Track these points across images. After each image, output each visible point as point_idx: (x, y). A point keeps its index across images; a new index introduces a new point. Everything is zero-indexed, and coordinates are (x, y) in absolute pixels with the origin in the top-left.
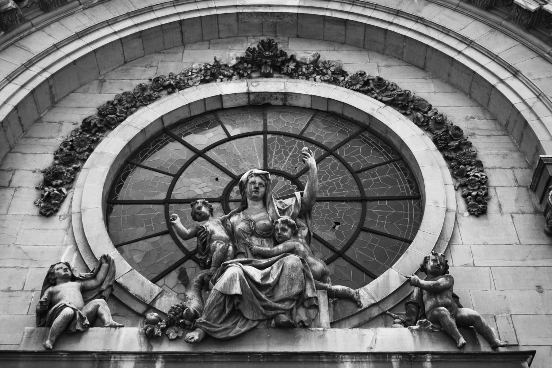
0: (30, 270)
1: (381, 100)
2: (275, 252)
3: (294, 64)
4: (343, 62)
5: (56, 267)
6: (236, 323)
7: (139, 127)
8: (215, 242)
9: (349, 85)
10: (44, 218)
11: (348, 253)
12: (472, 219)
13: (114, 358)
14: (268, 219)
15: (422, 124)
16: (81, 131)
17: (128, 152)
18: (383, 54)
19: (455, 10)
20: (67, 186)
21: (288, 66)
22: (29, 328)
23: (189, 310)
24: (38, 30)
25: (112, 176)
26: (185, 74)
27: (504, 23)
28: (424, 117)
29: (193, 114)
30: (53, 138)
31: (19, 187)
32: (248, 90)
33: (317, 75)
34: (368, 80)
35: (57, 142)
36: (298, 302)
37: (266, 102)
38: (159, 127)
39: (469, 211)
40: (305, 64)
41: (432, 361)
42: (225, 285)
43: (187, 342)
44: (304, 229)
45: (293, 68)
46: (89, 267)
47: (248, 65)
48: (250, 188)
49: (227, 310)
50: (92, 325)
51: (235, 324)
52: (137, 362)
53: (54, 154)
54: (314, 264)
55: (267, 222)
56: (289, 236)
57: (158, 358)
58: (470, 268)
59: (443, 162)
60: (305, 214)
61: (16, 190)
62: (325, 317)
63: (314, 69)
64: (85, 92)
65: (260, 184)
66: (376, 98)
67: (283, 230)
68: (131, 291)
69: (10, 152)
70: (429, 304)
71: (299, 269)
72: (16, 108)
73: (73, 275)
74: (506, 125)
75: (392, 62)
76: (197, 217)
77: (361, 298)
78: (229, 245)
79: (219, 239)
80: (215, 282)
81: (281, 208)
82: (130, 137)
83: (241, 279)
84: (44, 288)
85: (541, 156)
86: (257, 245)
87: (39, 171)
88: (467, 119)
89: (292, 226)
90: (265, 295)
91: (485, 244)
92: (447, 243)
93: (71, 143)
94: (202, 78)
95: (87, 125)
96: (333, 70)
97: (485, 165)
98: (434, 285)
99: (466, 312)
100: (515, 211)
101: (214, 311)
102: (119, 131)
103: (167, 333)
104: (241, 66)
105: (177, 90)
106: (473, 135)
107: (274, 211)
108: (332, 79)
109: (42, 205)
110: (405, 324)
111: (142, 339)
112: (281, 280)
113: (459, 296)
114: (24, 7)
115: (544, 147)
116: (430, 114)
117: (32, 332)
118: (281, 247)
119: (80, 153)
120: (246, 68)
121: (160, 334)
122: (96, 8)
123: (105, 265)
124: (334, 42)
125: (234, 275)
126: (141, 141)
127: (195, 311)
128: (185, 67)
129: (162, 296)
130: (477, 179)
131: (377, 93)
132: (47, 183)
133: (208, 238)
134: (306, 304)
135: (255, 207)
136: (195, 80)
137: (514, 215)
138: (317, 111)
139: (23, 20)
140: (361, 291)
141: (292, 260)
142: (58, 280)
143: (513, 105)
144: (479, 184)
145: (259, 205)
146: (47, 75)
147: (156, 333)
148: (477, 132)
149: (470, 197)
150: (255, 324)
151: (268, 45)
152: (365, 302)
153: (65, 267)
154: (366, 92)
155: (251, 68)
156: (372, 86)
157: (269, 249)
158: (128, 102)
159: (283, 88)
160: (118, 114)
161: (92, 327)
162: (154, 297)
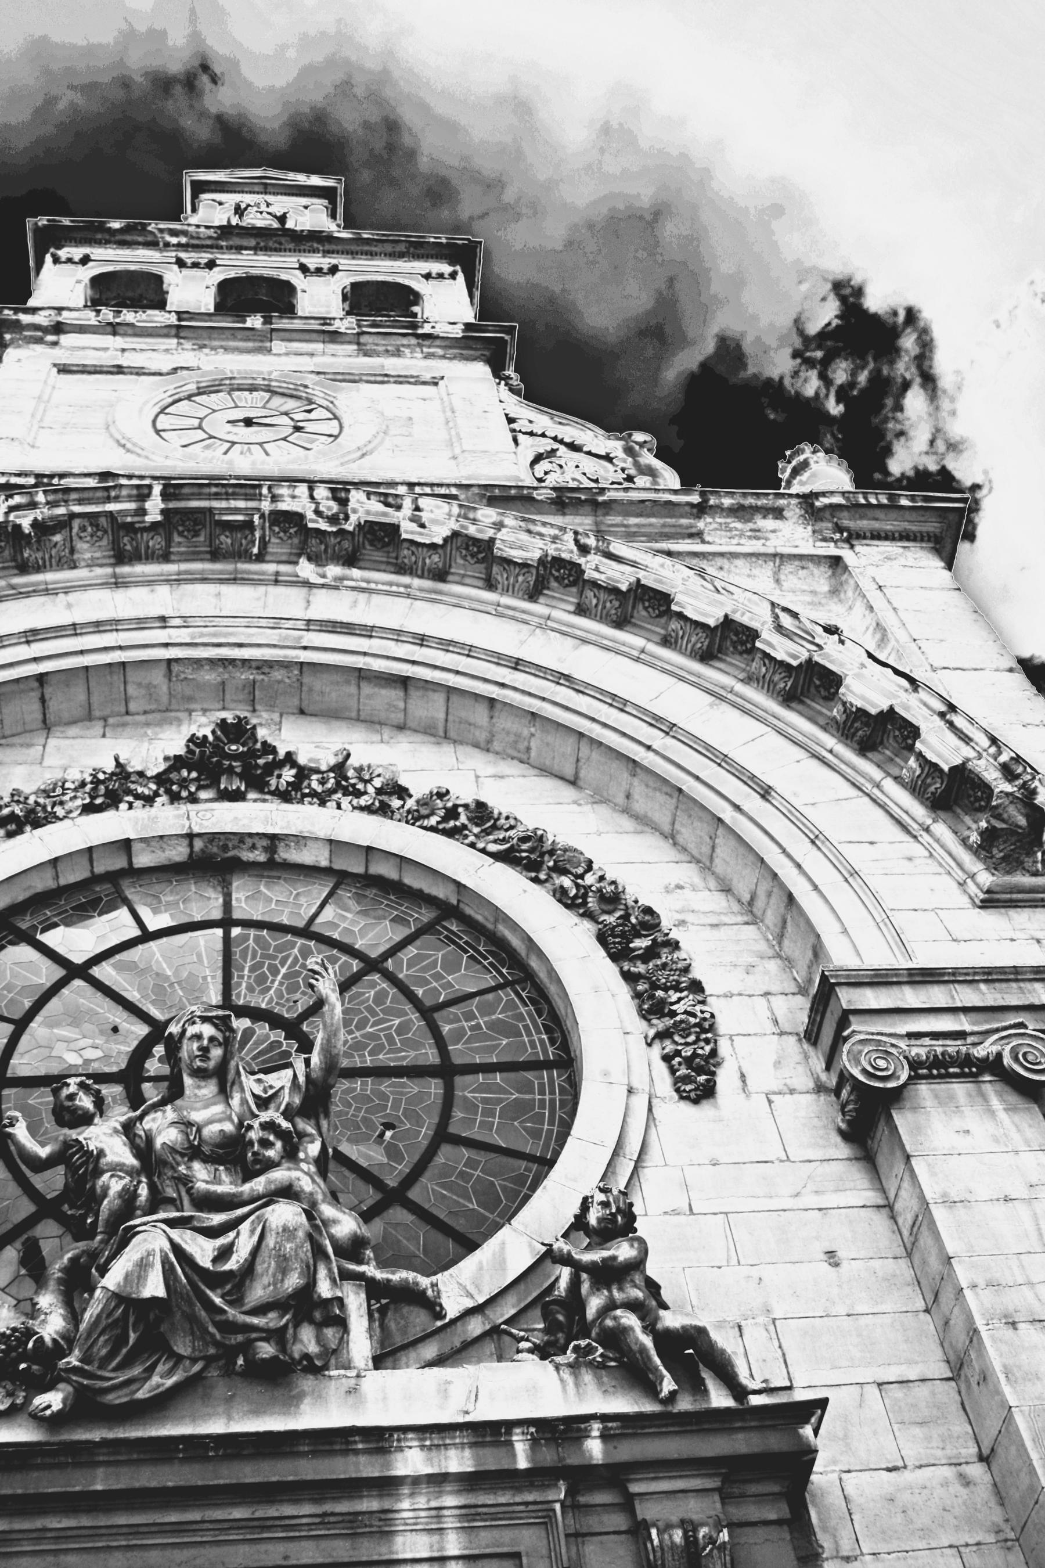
1: (483, 851)
2: (245, 1197)
3: (293, 772)
9: (414, 818)
18: (488, 750)
21: (279, 776)
28: (577, 886)
33: (344, 795)
40: (317, 771)
41: (604, 1437)
44: (312, 1142)
48: (188, 1049)
51: (150, 1371)
55: (229, 1127)
58: (682, 1219)
63: (338, 783)
65: (212, 1039)
66: (472, 845)
67: (265, 1144)
70: (594, 1304)
71: (301, 1234)
74: (751, 902)
76: (67, 1117)
78: (139, 1182)
79: (116, 1168)
80: (103, 1271)
83: (165, 1261)
90: (222, 1297)
92: (632, 1164)
94: (87, 801)
97: (708, 989)
101: (102, 1339)
104: (174, 776)
107: (244, 1102)
108: (377, 804)
110: (543, 1352)
112: (259, 1260)
116: (590, 879)
120: (185, 780)
127: (54, 1340)
131: (476, 835)
136: (70, 805)
145: (209, 1089)
148: (689, 918)
149: (678, 1059)
152: (453, 1307)
154: (450, 833)
155: (197, 779)
156: (463, 819)
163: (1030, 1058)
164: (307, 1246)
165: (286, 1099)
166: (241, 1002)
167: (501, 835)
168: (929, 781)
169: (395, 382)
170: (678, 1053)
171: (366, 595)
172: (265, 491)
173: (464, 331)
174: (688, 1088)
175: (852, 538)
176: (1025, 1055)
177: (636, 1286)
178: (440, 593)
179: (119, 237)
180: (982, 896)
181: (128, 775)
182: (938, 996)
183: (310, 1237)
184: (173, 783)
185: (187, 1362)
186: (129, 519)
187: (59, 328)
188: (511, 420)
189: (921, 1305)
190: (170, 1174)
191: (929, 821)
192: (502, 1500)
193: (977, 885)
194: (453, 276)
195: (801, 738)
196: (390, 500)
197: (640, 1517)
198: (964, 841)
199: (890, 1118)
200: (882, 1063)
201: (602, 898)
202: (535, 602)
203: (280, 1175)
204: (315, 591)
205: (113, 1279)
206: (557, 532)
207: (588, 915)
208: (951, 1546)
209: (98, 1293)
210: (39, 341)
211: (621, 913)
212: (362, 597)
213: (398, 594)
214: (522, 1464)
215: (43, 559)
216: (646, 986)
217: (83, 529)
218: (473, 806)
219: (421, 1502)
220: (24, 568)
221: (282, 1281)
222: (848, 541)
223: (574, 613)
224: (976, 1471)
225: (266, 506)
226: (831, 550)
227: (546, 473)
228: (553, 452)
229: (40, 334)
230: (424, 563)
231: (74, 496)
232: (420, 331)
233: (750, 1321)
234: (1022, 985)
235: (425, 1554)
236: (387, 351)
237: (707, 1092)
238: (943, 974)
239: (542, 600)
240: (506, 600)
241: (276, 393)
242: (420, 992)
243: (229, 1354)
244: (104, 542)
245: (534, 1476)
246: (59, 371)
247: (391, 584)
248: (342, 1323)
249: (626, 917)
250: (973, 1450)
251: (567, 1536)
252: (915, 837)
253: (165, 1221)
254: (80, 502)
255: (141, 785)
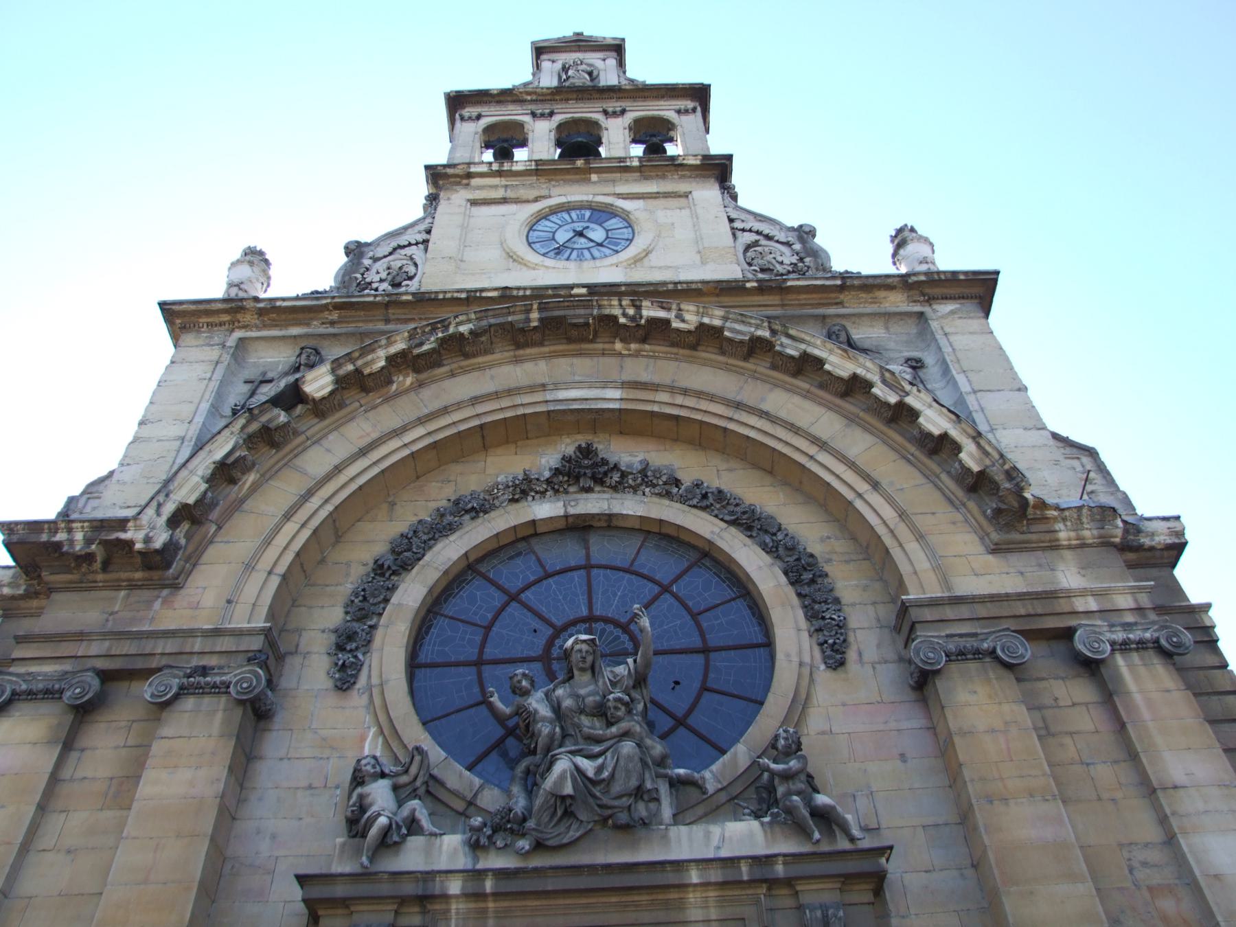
0: (331, 761)
1: (722, 520)
2: (608, 736)
3: (619, 475)
4: (676, 467)
5: (363, 762)
6: (571, 825)
7: (441, 568)
8: (539, 725)
9: (683, 500)
10: (340, 692)
11: (690, 721)
12: (829, 674)
13: (440, 877)
14: (598, 694)
15: (771, 550)
16: (373, 575)
17: (430, 601)
18: (723, 453)
19: (805, 397)
20: (363, 649)
21: (611, 478)
22: (340, 840)
23: (516, 813)
24: (314, 443)
25: (414, 633)
26: (489, 492)
27: (862, 414)
28: (773, 540)
29: (501, 544)
30: (341, 585)
31: (308, 653)
32: (566, 511)
33: (647, 487)
34: (707, 493)
35: (347, 587)
36: (636, 795)
37: (587, 524)
38: (464, 564)
39: (825, 663)
40: (632, 473)
41: (784, 863)
42: (555, 783)
43: (517, 853)
44: (639, 703)
45: (618, 480)
46: (398, 755)
47: (563, 477)
48: (575, 657)
49: (559, 813)
50: (410, 833)
52: (465, 881)
53: (344, 607)
54: (653, 748)
55: (598, 698)
56: (623, 716)
57: (487, 875)
58: (826, 736)
59: (795, 600)
60: (639, 683)
61: (305, 658)
62: (667, 812)
63: (643, 480)
64: (373, 520)
65: (587, 652)
66: (716, 516)
67: (616, 708)
68: (448, 786)
69: (293, 606)
70: (781, 790)
71: (636, 758)
72: (298, 554)
73: (382, 771)
74: (868, 547)
75: (734, 464)
76: (518, 691)
77: (707, 782)
78: (555, 726)
79: (544, 719)
80: (543, 777)
81: (612, 679)
82: (431, 582)
83: (572, 775)
84: (352, 787)
85: (903, 597)
86: (588, 727)
87: (329, 631)
88: (822, 540)
89: (626, 704)
90: (600, 791)
91: (844, 705)
92: (801, 707)
93: (362, 593)
94: (511, 497)
95: (379, 569)
96: (665, 480)
97: (844, 601)
98: (784, 770)
99: (822, 799)
100: (877, 660)
101: (545, 814)
102: (417, 574)
103: (494, 841)
104: (555, 480)
105: (481, 514)
106: (829, 561)
107: (605, 683)
108: (664, 492)
109: (337, 676)
110: (757, 816)
111: (467, 849)
112: (616, 772)
113: (814, 776)
114: (297, 417)
115: (906, 583)
116: (780, 536)
117: (343, 845)
118: (614, 729)
119: (375, 604)
120: (561, 482)
121: (486, 844)
122: (380, 409)
123: (417, 758)
124: (664, 438)
125: (564, 772)
126: (444, 583)
127: (523, 813)
128: (490, 482)
129: (483, 789)
130: (833, 622)
131: (718, 509)
132: (340, 648)
133: (532, 719)
134: (646, 797)
135: (582, 678)
136: (502, 498)
137: (877, 666)
138: (649, 532)
139: (296, 433)
140: (707, 774)
141: (628, 747)
142: (367, 779)
143: (872, 528)
144: (836, 628)
145: (587, 677)
146: (329, 508)
147: (482, 843)
148: (834, 557)
149: (826, 645)
150: (590, 827)
151: (586, 451)
152: (711, 787)
153: (373, 761)
154: (704, 509)
155: (568, 481)
156: (711, 500)
157: (601, 732)
158: (425, 534)
159: (606, 508)
160: (414, 550)
161: (411, 835)
162: (474, 792)
163: (1011, 650)
164: (639, 765)
165: (626, 683)
166: (598, 613)
167: (731, 508)
168: (966, 476)
169: (663, 197)
170: (826, 642)
171: (653, 360)
172: (595, 303)
173: (702, 160)
174: (831, 662)
175: (930, 300)
176: (1008, 647)
177: (802, 782)
178: (695, 357)
179: (497, 99)
180: (992, 547)
181: (531, 481)
182: (964, 611)
183: (641, 759)
184: (555, 484)
185: (585, 824)
186: (521, 325)
187: (469, 175)
188: (731, 220)
189: (947, 783)
190: (570, 721)
191: (965, 500)
192: (736, 893)
193: (990, 539)
194: (694, 110)
195: (896, 446)
196: (664, 305)
197: (801, 902)
198: (984, 513)
199: (934, 683)
200: (931, 655)
201: (787, 549)
202: (748, 362)
203: (624, 725)
204: (625, 359)
205: (549, 783)
206: (758, 322)
207: (778, 557)
208: (954, 911)
209: (542, 791)
210: (459, 184)
211: (797, 557)
212: (652, 361)
213: (670, 359)
214: (745, 878)
215: (477, 351)
216: (810, 601)
217: (496, 331)
218: (716, 493)
219: (698, 895)
220: (467, 356)
221: (629, 782)
222: (928, 301)
223: (770, 368)
224: (970, 872)
225: (595, 312)
226: (917, 308)
227: (752, 259)
228: (756, 244)
229: (458, 179)
230: (685, 341)
231: (490, 313)
232: (676, 163)
233: (860, 793)
234: (1010, 602)
235: (701, 919)
236: (657, 175)
237: (842, 663)
238: (967, 599)
239: (752, 360)
240: (731, 361)
241: (595, 210)
242: (690, 604)
243: (604, 820)
244: (509, 337)
245: (753, 882)
246: (471, 204)
247: (667, 353)
248: (657, 800)
249: (798, 559)
250: (969, 861)
251: (767, 910)
252: (957, 509)
253: (571, 752)
254: (494, 316)
255: (539, 486)
